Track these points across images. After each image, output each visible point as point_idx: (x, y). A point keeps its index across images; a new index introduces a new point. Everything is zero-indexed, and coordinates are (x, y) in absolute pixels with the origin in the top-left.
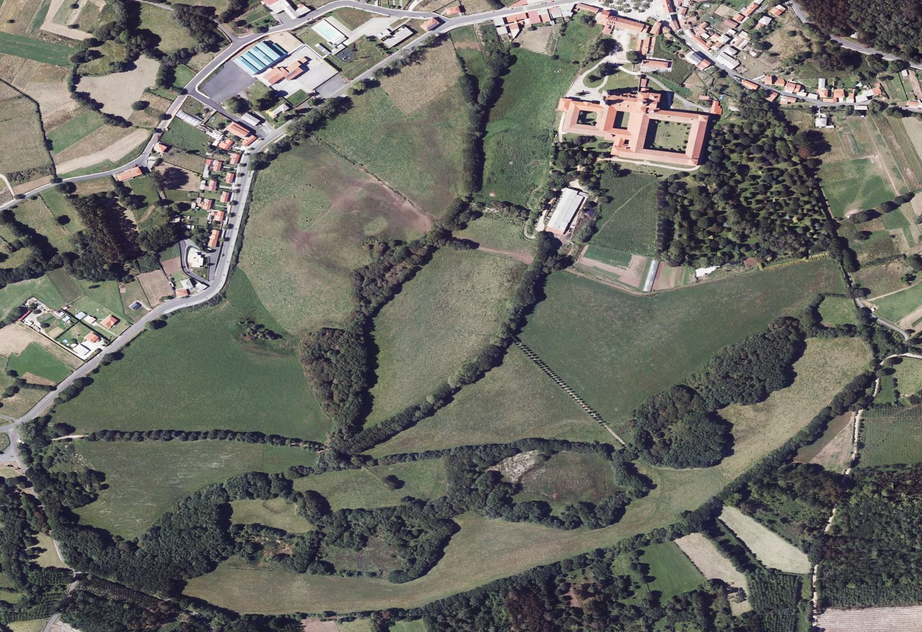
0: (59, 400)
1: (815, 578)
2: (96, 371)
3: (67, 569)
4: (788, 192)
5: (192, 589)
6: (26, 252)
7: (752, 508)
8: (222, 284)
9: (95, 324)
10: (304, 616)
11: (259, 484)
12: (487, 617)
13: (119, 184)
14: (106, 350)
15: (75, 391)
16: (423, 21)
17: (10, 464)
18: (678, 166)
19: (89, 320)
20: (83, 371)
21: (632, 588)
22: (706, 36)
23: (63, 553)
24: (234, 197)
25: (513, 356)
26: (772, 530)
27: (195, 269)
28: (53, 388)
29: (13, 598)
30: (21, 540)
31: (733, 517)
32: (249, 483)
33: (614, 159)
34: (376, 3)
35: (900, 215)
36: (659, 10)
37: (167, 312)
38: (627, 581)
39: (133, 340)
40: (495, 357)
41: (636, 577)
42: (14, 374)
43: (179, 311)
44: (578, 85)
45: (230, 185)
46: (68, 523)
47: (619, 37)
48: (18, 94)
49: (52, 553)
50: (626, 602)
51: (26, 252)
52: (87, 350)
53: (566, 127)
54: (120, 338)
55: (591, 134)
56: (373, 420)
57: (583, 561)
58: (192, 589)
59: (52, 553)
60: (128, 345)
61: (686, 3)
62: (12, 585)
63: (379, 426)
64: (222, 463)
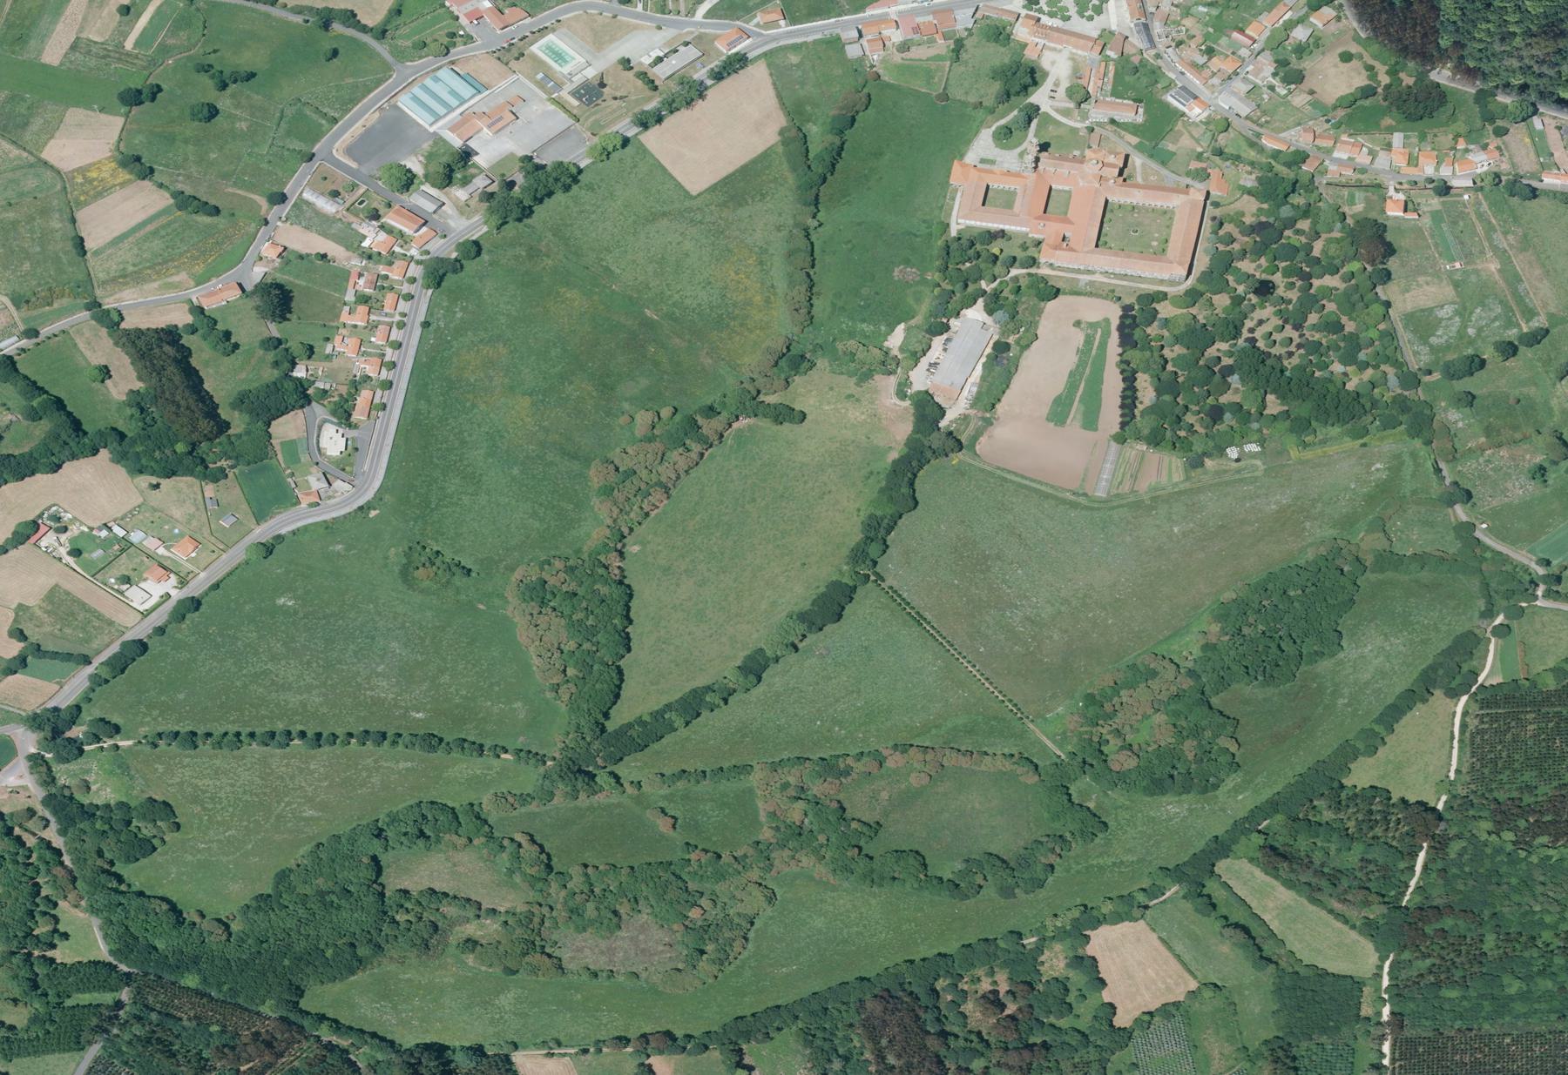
0: (97, 681)
1: (1386, 982)
2: (160, 631)
3: (110, 964)
4: (1336, 327)
5: (319, 997)
6: (43, 428)
7: (1276, 857)
8: (377, 484)
9: (161, 551)
10: (516, 1046)
11: (429, 824)
12: (827, 1046)
13: (199, 311)
14: (176, 595)
15: (119, 664)
16: (716, 37)
17: (10, 786)
18: (1125, 277)
19: (151, 544)
20: (141, 631)
21: (1071, 998)
22: (1201, 60)
23: (106, 937)
24: (396, 335)
25: (864, 609)
26: (1314, 901)
27: (330, 459)
28: (87, 661)
29: (18, 1017)
30: (31, 914)
31: (1244, 877)
32: (424, 817)
33: (1044, 271)
34: (640, 6)
35: (534, 58)
36: (1118, 16)
37: (283, 531)
38: (1063, 984)
39: (230, 574)
40: (831, 606)
41: (1077, 978)
42: (19, 634)
43: (306, 528)
44: (983, 144)
45: (392, 316)
46: (110, 889)
47: (1053, 63)
48: (32, 159)
49: (85, 936)
50: (1063, 1023)
51: (43, 428)
52: (152, 594)
53: (963, 218)
54: (202, 575)
55: (995, 226)
56: (621, 715)
57: (984, 951)
58: (319, 997)
59: (85, 936)
60: (216, 586)
61: (1166, 7)
62: (17, 993)
63: (647, 718)
64: (392, 779)
